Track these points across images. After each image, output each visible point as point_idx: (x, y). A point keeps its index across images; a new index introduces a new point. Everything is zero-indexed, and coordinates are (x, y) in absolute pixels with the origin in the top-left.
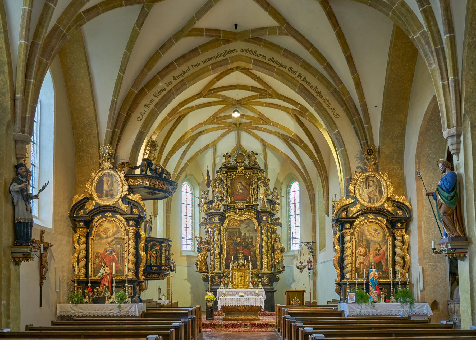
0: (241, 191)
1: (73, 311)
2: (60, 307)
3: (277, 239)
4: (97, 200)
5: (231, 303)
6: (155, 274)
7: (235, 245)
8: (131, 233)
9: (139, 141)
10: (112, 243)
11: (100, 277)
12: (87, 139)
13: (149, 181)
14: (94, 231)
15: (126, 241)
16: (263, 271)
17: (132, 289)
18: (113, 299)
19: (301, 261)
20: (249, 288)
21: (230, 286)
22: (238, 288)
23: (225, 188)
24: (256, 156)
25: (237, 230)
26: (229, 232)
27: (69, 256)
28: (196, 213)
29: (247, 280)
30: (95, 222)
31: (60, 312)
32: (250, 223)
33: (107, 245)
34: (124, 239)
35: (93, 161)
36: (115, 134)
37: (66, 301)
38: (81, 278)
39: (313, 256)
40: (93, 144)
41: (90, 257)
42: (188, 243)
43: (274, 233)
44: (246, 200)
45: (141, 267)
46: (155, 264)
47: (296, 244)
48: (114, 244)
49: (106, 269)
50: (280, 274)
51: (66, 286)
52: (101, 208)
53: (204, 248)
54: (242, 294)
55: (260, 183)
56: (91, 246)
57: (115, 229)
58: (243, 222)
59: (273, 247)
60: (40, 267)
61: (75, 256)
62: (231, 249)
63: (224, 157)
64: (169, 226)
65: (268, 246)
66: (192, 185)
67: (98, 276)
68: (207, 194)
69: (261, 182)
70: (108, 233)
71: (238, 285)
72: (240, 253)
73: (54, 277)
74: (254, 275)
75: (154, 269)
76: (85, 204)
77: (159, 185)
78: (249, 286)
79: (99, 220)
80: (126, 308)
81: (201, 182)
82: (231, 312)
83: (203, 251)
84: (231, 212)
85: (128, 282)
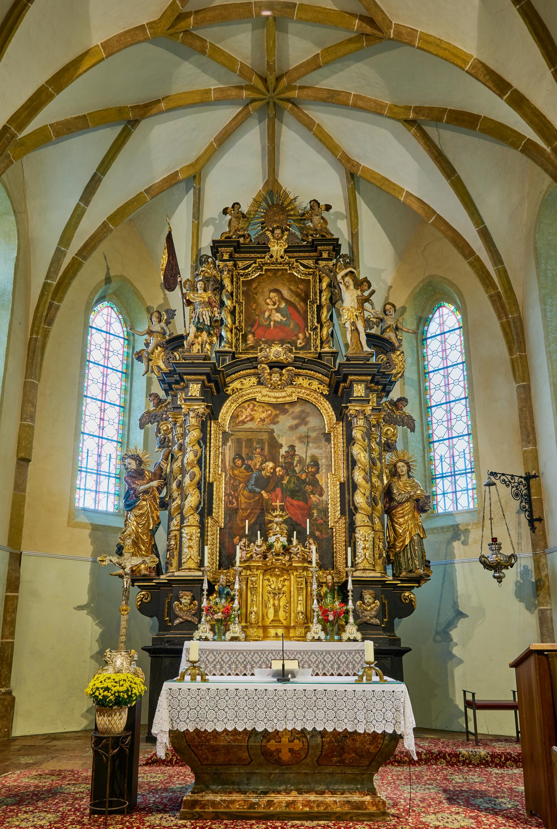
0: (278, 317)
3: (400, 464)
5: (231, 713)
7: (256, 485)
16: (357, 574)
19: (494, 540)
20: (309, 636)
21: (236, 629)
22: (266, 637)
23: (228, 303)
24: (325, 214)
25: (265, 436)
26: (239, 441)
28: (135, 395)
29: (301, 608)
32: (308, 414)
39: (531, 522)
42: (103, 487)
43: (389, 447)
44: (294, 343)
47: (455, 492)
50: (415, 591)
53: (146, 492)
54: (291, 665)
55: (343, 278)
58: (285, 412)
59: (388, 492)
62: (242, 499)
63: (229, 217)
64: (32, 418)
65: (373, 486)
66: (128, 314)
68: (168, 323)
69: (346, 275)
71: (265, 628)
72: (274, 510)
74: (325, 589)
78: (308, 629)
82: (229, 764)
83: (145, 504)
84: (244, 377)
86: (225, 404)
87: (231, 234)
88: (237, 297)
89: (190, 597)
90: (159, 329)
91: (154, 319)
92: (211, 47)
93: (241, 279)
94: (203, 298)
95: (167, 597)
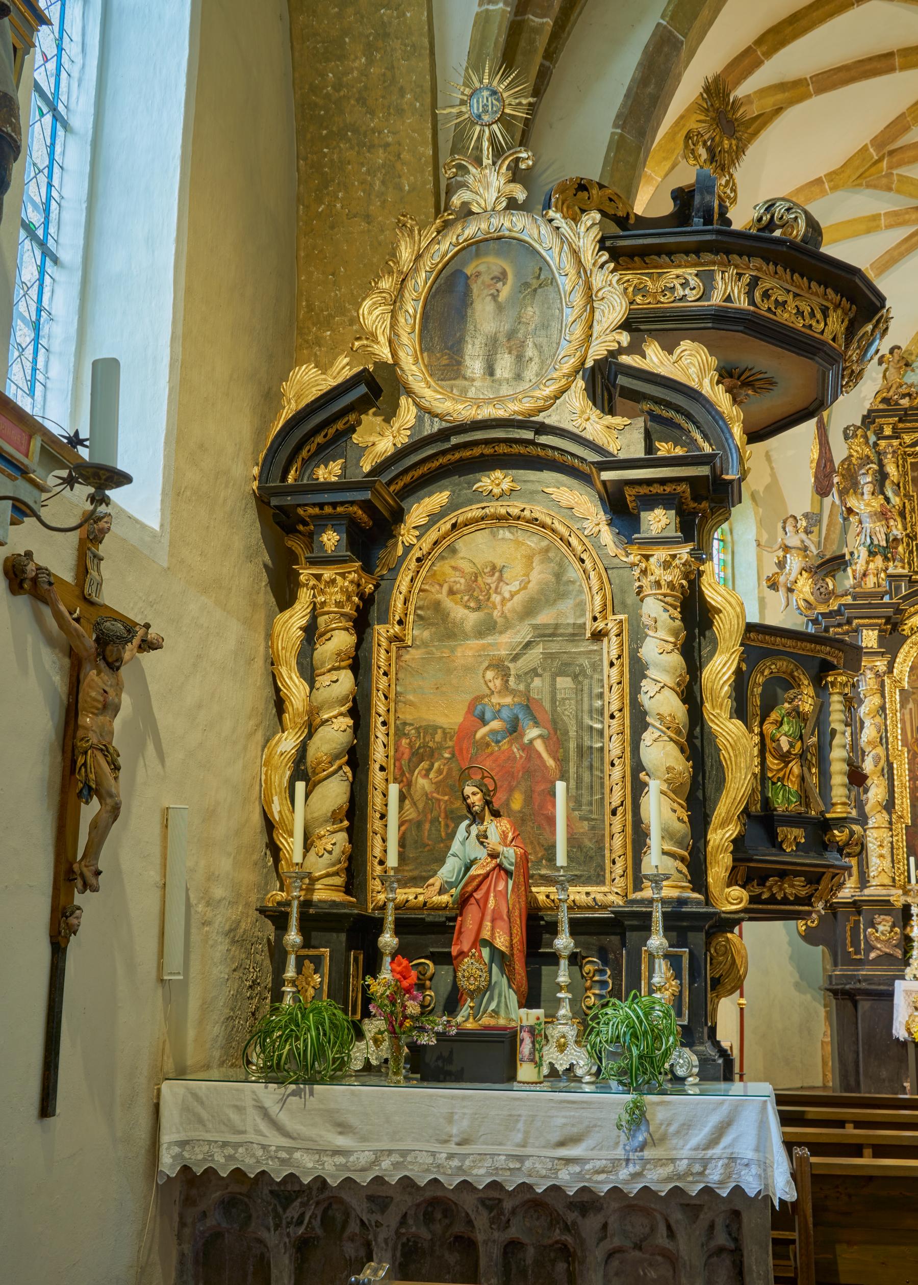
1: (275, 1140)
2: (186, 1109)
4: (428, 393)
6: (797, 874)
8: (658, 584)
9: (651, 89)
10: (520, 663)
11: (451, 885)
12: (371, 62)
13: (746, 279)
14: (404, 588)
15: (611, 648)
17: (678, 976)
18: (562, 1048)
27: (245, 748)
30: (407, 534)
31: (183, 1144)
33: (490, 675)
34: (598, 636)
35: (399, 188)
36: (523, 44)
37: (217, 1054)
38: (320, 895)
40: (402, 92)
41: (378, 754)
45: (723, 824)
46: (794, 806)
48: (534, 672)
49: (495, 829)
51: (222, 946)
52: (454, 440)
56: (383, 682)
57: (539, 575)
60: (64, 790)
61: (280, 749)
67: (436, 881)
70: (496, 598)
73: (153, 875)
75: (793, 835)
76: (352, 417)
77: (800, 313)
79: (434, 518)
80: (687, 1127)
81: (761, 490)
85: (667, 929)
86: (902, 650)
87: (891, 393)
88: (905, 489)
89: (890, 924)
90: (798, 543)
91: (789, 528)
92: (898, 181)
93: (909, 461)
94: (873, 506)
95: (849, 921)
